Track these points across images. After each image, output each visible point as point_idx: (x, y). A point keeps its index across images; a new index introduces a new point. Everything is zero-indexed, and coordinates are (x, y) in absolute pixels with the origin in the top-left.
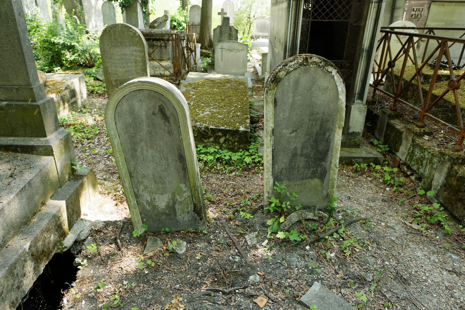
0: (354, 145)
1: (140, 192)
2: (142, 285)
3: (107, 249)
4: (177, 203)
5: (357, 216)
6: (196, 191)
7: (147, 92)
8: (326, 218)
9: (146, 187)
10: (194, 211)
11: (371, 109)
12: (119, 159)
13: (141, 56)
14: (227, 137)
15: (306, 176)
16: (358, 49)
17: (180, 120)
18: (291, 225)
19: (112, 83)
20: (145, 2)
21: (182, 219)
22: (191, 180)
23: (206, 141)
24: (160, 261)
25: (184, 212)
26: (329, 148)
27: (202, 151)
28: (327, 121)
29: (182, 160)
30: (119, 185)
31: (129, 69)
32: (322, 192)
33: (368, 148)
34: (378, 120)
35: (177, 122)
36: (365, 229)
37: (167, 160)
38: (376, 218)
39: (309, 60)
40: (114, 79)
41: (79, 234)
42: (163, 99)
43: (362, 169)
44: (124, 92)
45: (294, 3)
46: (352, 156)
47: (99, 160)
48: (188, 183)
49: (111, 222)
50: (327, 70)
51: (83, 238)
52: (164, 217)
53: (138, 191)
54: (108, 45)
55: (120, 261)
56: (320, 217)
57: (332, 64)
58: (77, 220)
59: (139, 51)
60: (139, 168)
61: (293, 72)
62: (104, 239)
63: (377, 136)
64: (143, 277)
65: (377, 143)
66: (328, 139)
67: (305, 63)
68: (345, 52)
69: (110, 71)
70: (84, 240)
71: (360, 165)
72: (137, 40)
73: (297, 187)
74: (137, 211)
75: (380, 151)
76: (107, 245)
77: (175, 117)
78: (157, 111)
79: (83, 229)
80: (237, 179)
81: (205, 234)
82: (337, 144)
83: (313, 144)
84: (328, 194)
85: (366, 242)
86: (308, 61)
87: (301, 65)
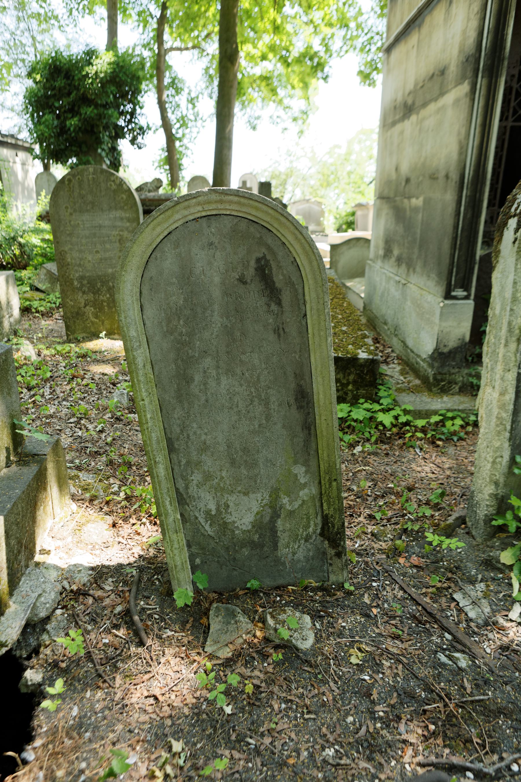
1: (193, 490)
2: (227, 752)
4: (282, 516)
7: (228, 223)
9: (208, 477)
12: (146, 402)
17: (307, 298)
19: (72, 284)
20: (115, 165)
21: (290, 556)
22: (323, 454)
24: (257, 673)
25: (296, 538)
29: (304, 404)
30: (112, 481)
31: (107, 255)
37: (267, 404)
41: (35, 604)
42: (270, 241)
44: (171, 221)
45: (485, 81)
47: (58, 427)
48: (313, 463)
49: (108, 567)
51: (43, 614)
52: (246, 552)
53: (187, 487)
54: (67, 208)
55: (147, 676)
58: (27, 566)
59: (129, 220)
60: (195, 425)
62: (97, 614)
64: (222, 726)
69: (69, 260)
70: (47, 619)
72: (124, 197)
74: (179, 540)
76: (108, 631)
77: (296, 290)
78: (251, 272)
79: (44, 591)
81: (349, 593)
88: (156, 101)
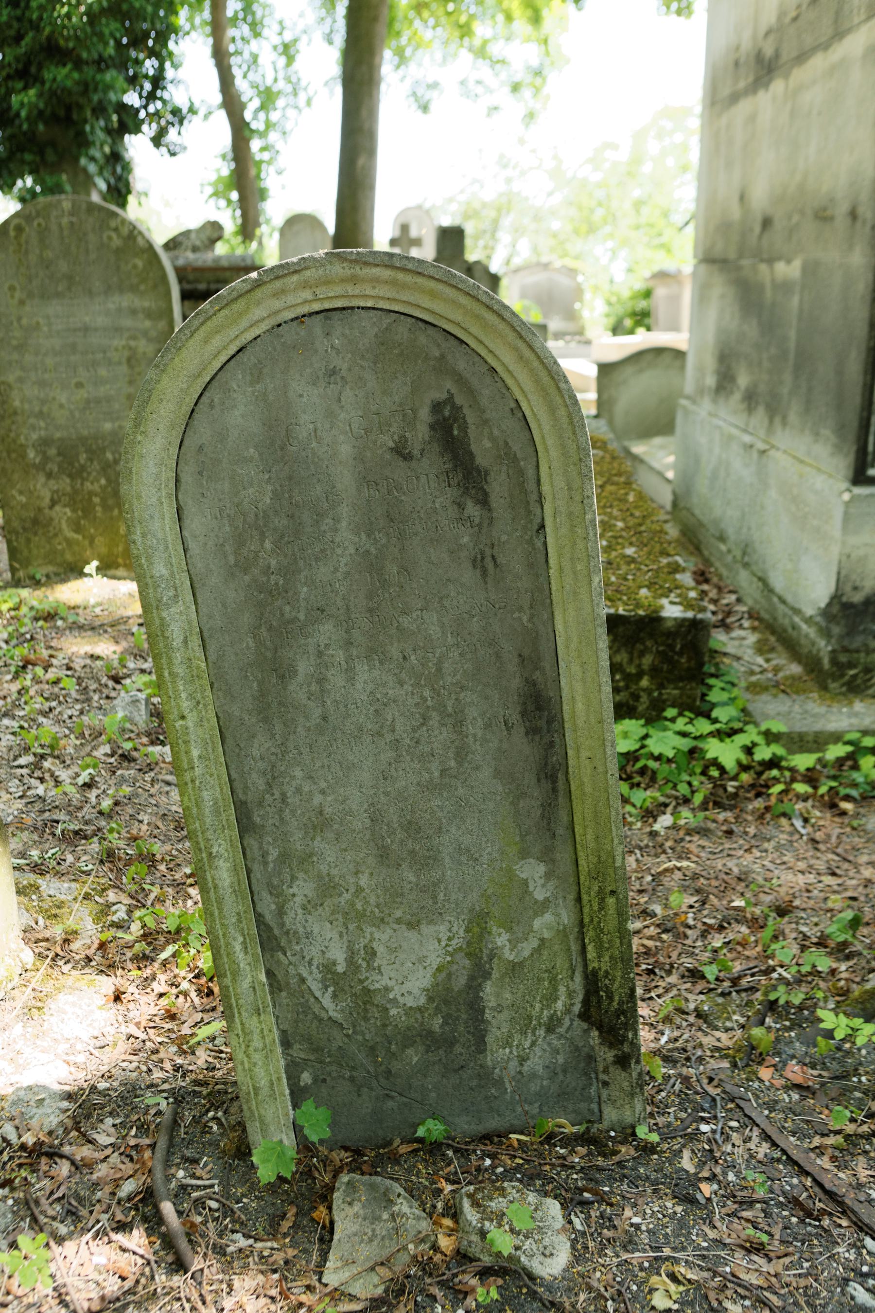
1: (294, 917)
3: (103, 1260)
4: (495, 975)
6: (611, 901)
7: (369, 325)
9: (328, 888)
10: (584, 1016)
12: (190, 722)
13: (153, 334)
17: (546, 488)
19: (24, 456)
21: (513, 1064)
22: (586, 835)
25: (526, 1025)
29: (542, 723)
31: (102, 391)
35: (528, 498)
37: (459, 724)
40: (35, 436)
42: (461, 365)
44: (244, 323)
52: (413, 1055)
53: (281, 912)
54: (12, 288)
59: (148, 314)
60: (298, 773)
69: (17, 403)
74: (263, 1029)
77: (521, 472)
78: (420, 433)
80: (693, 847)
81: (648, 1149)
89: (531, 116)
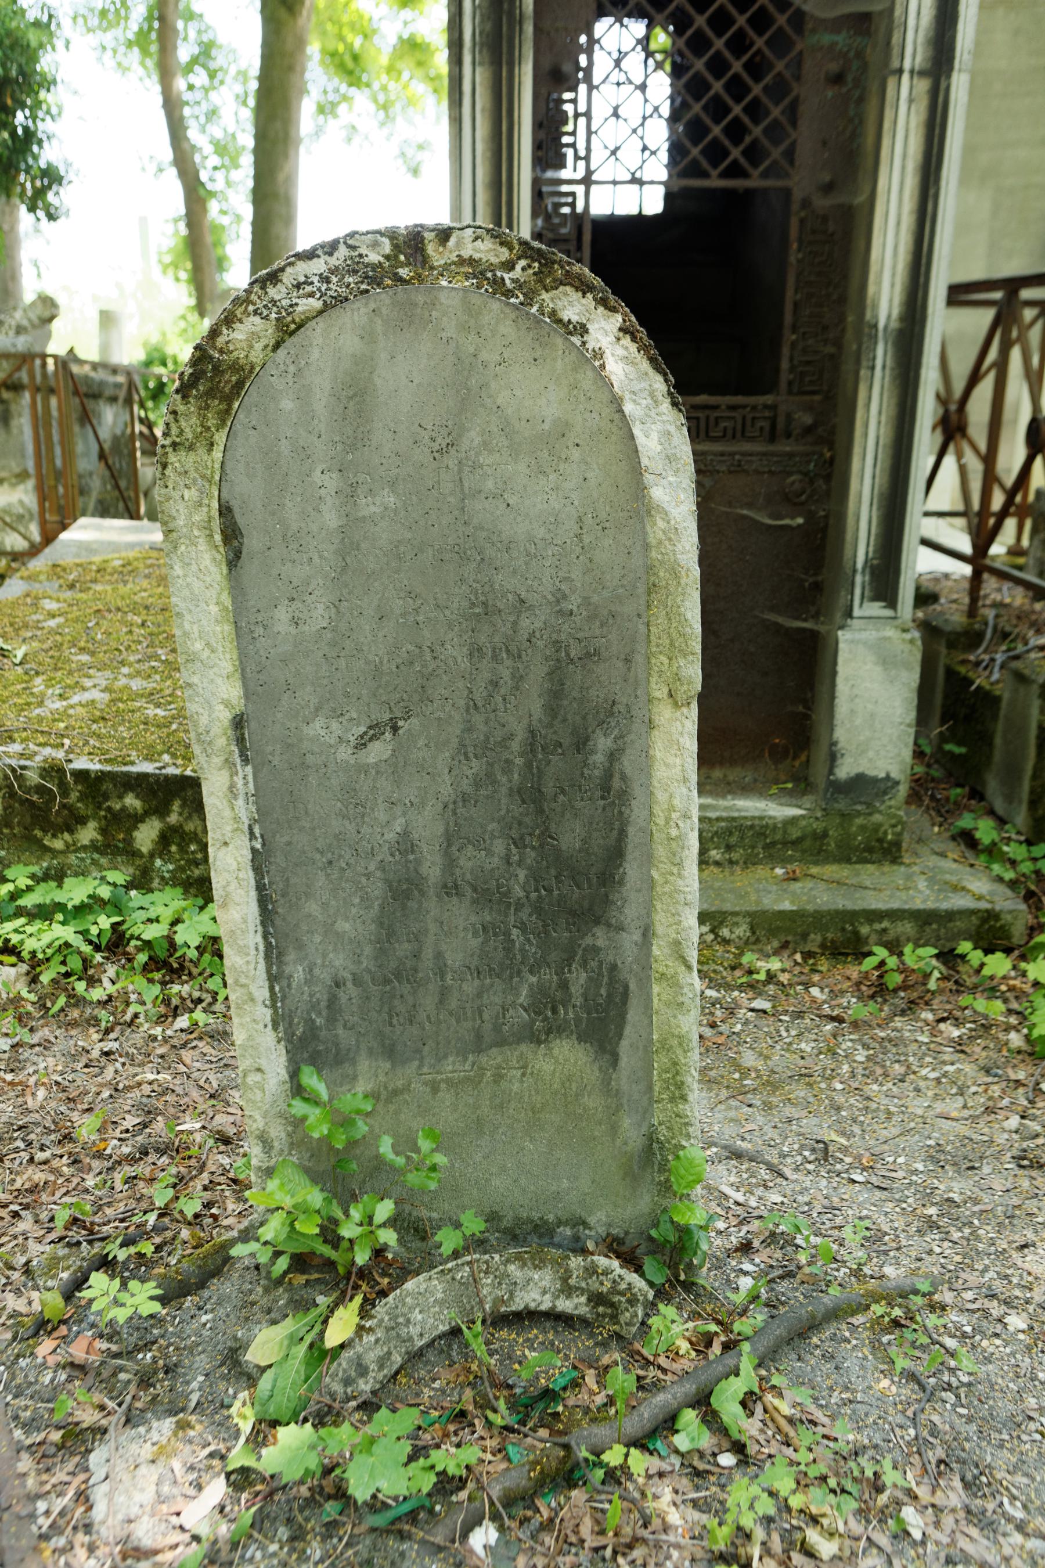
0: (870, 850)
5: (857, 1273)
8: (633, 1301)
11: (962, 670)
14: (173, 818)
15: (497, 1028)
16: (849, 334)
18: (397, 1359)
23: (58, 844)
26: (622, 833)
27: (28, 901)
28: (591, 656)
32: (614, 1129)
33: (948, 864)
34: (995, 717)
36: (902, 1363)
38: (973, 1278)
39: (430, 249)
43: (913, 978)
45: (482, 75)
46: (859, 905)
50: (553, 314)
56: (597, 1299)
57: (579, 277)
61: (319, 326)
63: (999, 806)
65: (994, 835)
66: (608, 775)
67: (404, 272)
68: (786, 351)
71: (900, 954)
73: (446, 1096)
75: (1009, 875)
82: (672, 809)
83: (517, 810)
84: (651, 1138)
85: (890, 1477)
86: (425, 260)
87: (376, 281)
88: (159, 100)
89: (421, 147)
